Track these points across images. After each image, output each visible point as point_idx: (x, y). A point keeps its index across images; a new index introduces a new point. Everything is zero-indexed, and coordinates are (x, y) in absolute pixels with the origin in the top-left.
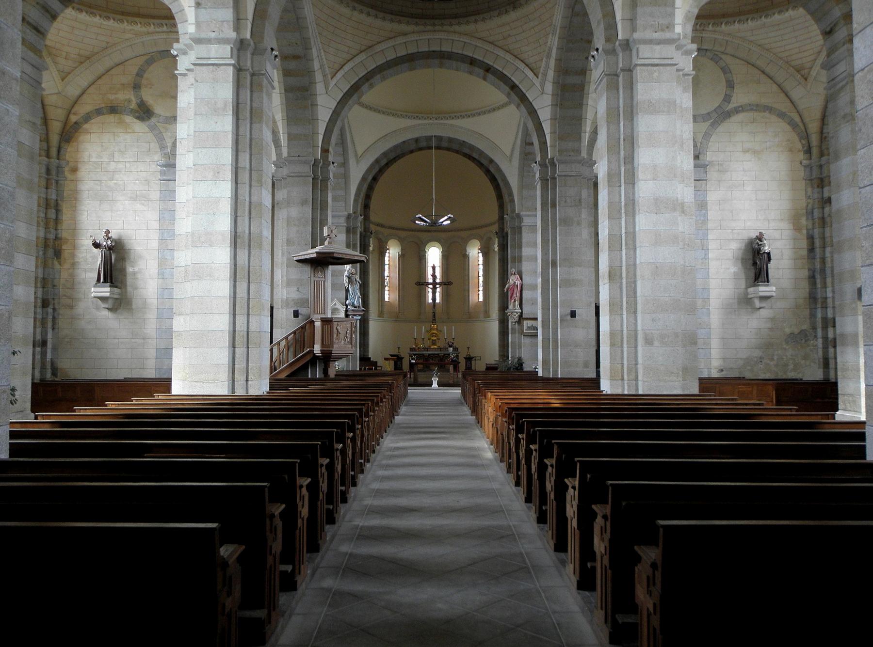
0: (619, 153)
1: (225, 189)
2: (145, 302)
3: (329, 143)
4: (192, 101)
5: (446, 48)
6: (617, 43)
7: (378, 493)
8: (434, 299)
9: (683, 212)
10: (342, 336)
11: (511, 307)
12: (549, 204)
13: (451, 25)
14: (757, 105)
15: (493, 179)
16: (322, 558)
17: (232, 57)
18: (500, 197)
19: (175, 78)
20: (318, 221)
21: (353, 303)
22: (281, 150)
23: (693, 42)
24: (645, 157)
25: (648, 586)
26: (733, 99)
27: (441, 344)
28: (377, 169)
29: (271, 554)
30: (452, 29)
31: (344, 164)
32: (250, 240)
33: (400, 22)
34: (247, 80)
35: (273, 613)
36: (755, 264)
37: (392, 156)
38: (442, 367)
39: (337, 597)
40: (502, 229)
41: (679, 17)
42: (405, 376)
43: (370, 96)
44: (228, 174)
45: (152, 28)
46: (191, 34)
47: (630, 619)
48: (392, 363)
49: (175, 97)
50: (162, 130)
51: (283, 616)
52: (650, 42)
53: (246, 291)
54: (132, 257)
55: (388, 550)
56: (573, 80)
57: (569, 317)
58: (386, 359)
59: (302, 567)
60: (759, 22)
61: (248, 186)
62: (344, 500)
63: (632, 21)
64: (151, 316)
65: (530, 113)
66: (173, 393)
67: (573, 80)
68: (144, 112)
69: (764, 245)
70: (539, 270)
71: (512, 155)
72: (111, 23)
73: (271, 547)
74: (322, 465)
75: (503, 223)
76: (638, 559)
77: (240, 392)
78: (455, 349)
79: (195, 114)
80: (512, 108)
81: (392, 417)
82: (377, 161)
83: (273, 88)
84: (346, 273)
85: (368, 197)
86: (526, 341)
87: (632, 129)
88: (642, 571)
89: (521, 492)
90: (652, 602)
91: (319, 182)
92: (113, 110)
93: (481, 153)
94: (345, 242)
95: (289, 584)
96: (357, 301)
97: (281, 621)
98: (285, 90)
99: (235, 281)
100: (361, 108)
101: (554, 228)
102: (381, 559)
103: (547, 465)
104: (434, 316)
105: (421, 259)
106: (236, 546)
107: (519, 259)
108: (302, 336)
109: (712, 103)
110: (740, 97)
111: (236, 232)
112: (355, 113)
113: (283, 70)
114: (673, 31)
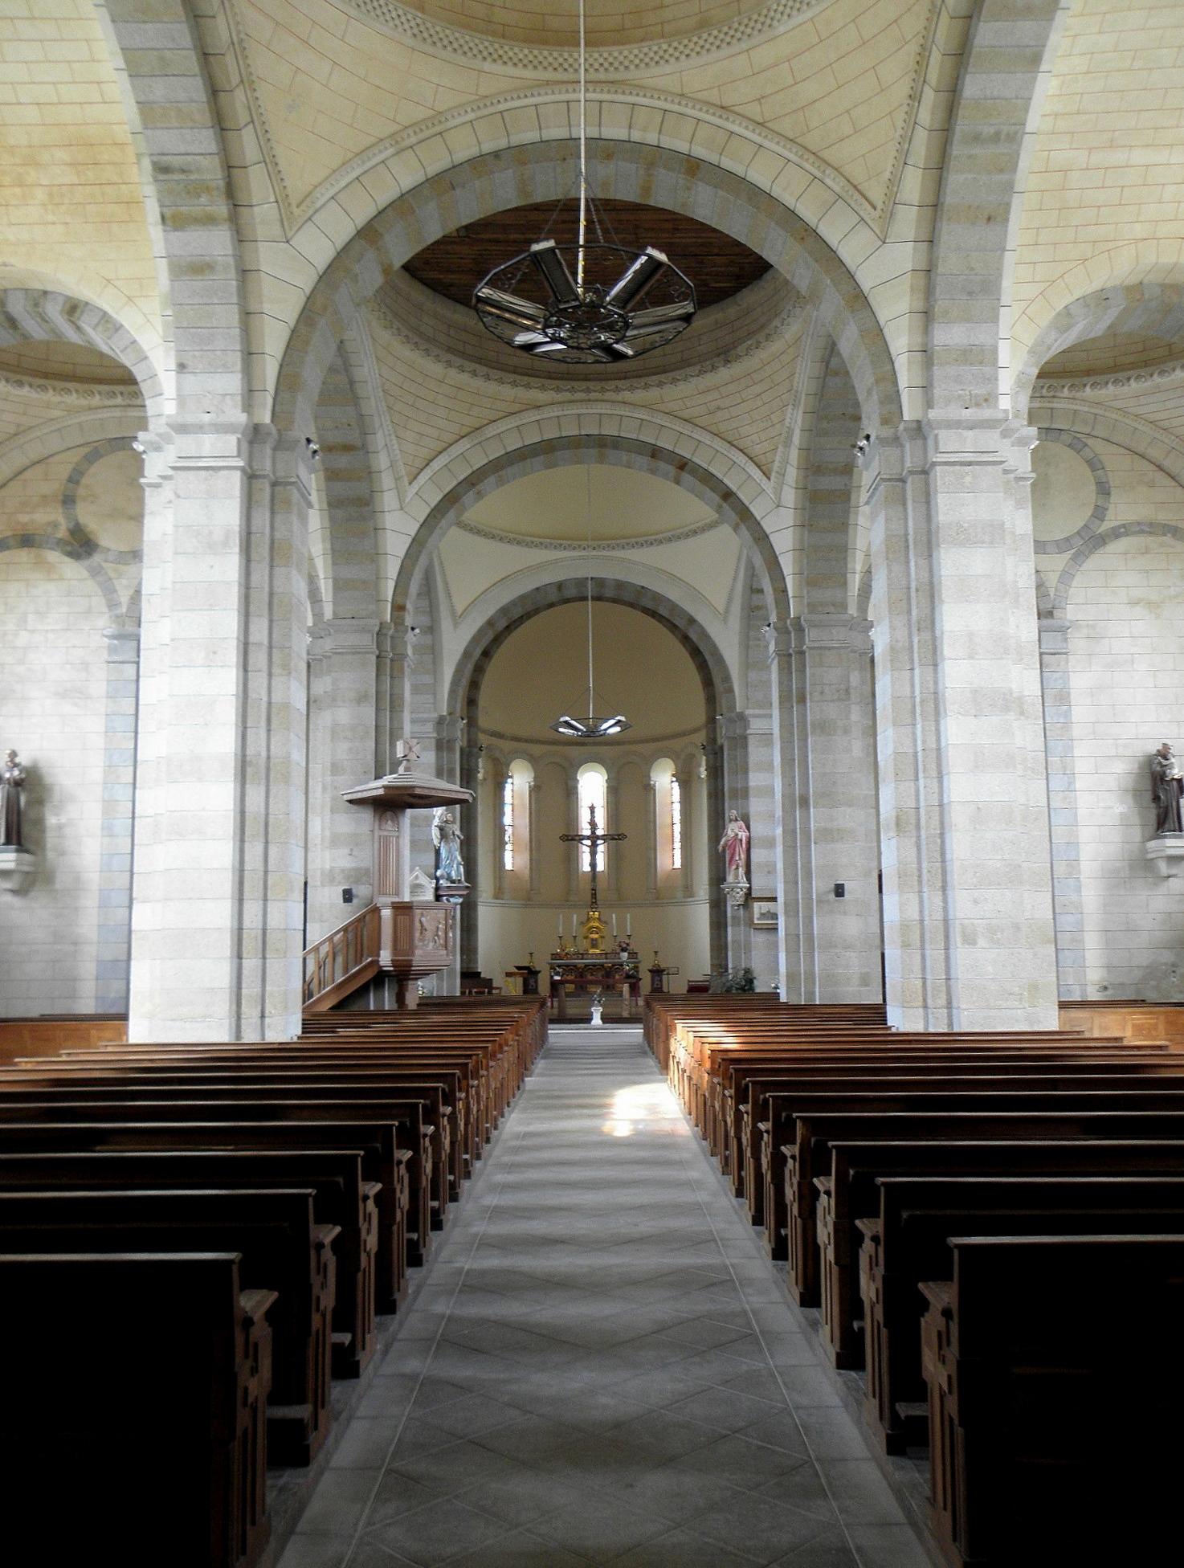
0: (909, 612)
1: (228, 680)
2: (77, 879)
3: (406, 595)
4: (170, 530)
5: (610, 430)
6: (901, 427)
7: (497, 1213)
8: (593, 865)
9: (1022, 713)
10: (429, 934)
11: (730, 878)
12: (794, 698)
13: (617, 390)
14: (1151, 525)
15: (696, 653)
16: (401, 1324)
17: (239, 456)
18: (708, 683)
19: (141, 488)
20: (385, 732)
21: (449, 875)
22: (321, 608)
23: (1030, 424)
24: (953, 619)
25: (940, 1347)
26: (1110, 514)
27: (606, 946)
28: (490, 635)
29: (318, 1310)
30: (620, 398)
31: (432, 629)
32: (268, 769)
33: (528, 386)
34: (265, 491)
35: (322, 1413)
36: (1156, 799)
37: (516, 613)
38: (609, 988)
39: (428, 1389)
40: (712, 740)
41: (1006, 381)
42: (543, 1005)
43: (477, 511)
44: (232, 655)
45: (96, 400)
46: (169, 416)
47: (915, 1410)
48: (520, 980)
49: (138, 518)
50: (112, 575)
51: (337, 1419)
52: (958, 425)
53: (261, 858)
54: (56, 796)
55: (514, 1309)
56: (828, 483)
57: (832, 896)
58: (509, 975)
59: (368, 1336)
60: (1149, 383)
61: (265, 675)
62: (437, 1225)
63: (927, 388)
64: (90, 902)
65: (757, 540)
66: (132, 1041)
67: (828, 483)
68: (81, 545)
69: (1171, 766)
70: (779, 813)
71: (727, 611)
72: (25, 391)
73: (318, 1298)
74: (400, 1162)
75: (714, 730)
76: (924, 1305)
77: (250, 1036)
78: (633, 955)
79: (176, 553)
80: (726, 529)
81: (521, 1078)
82: (490, 623)
83: (310, 505)
84: (436, 822)
85: (474, 685)
86: (759, 939)
87: (931, 571)
88: (931, 1324)
89: (746, 1208)
90: (945, 1374)
91: (387, 663)
92: (27, 541)
93: (674, 607)
94: (433, 766)
95: (347, 1366)
96: (457, 871)
97: (335, 1427)
98: (330, 504)
99: (242, 841)
100: (461, 531)
101: (804, 740)
102: (503, 1324)
103: (784, 1157)
104: (594, 896)
105: (570, 792)
106: (264, 1292)
107: (743, 793)
108: (359, 934)
109: (1070, 521)
110: (1121, 511)
111: (244, 756)
112: (452, 541)
113: (326, 470)
114: (996, 406)
